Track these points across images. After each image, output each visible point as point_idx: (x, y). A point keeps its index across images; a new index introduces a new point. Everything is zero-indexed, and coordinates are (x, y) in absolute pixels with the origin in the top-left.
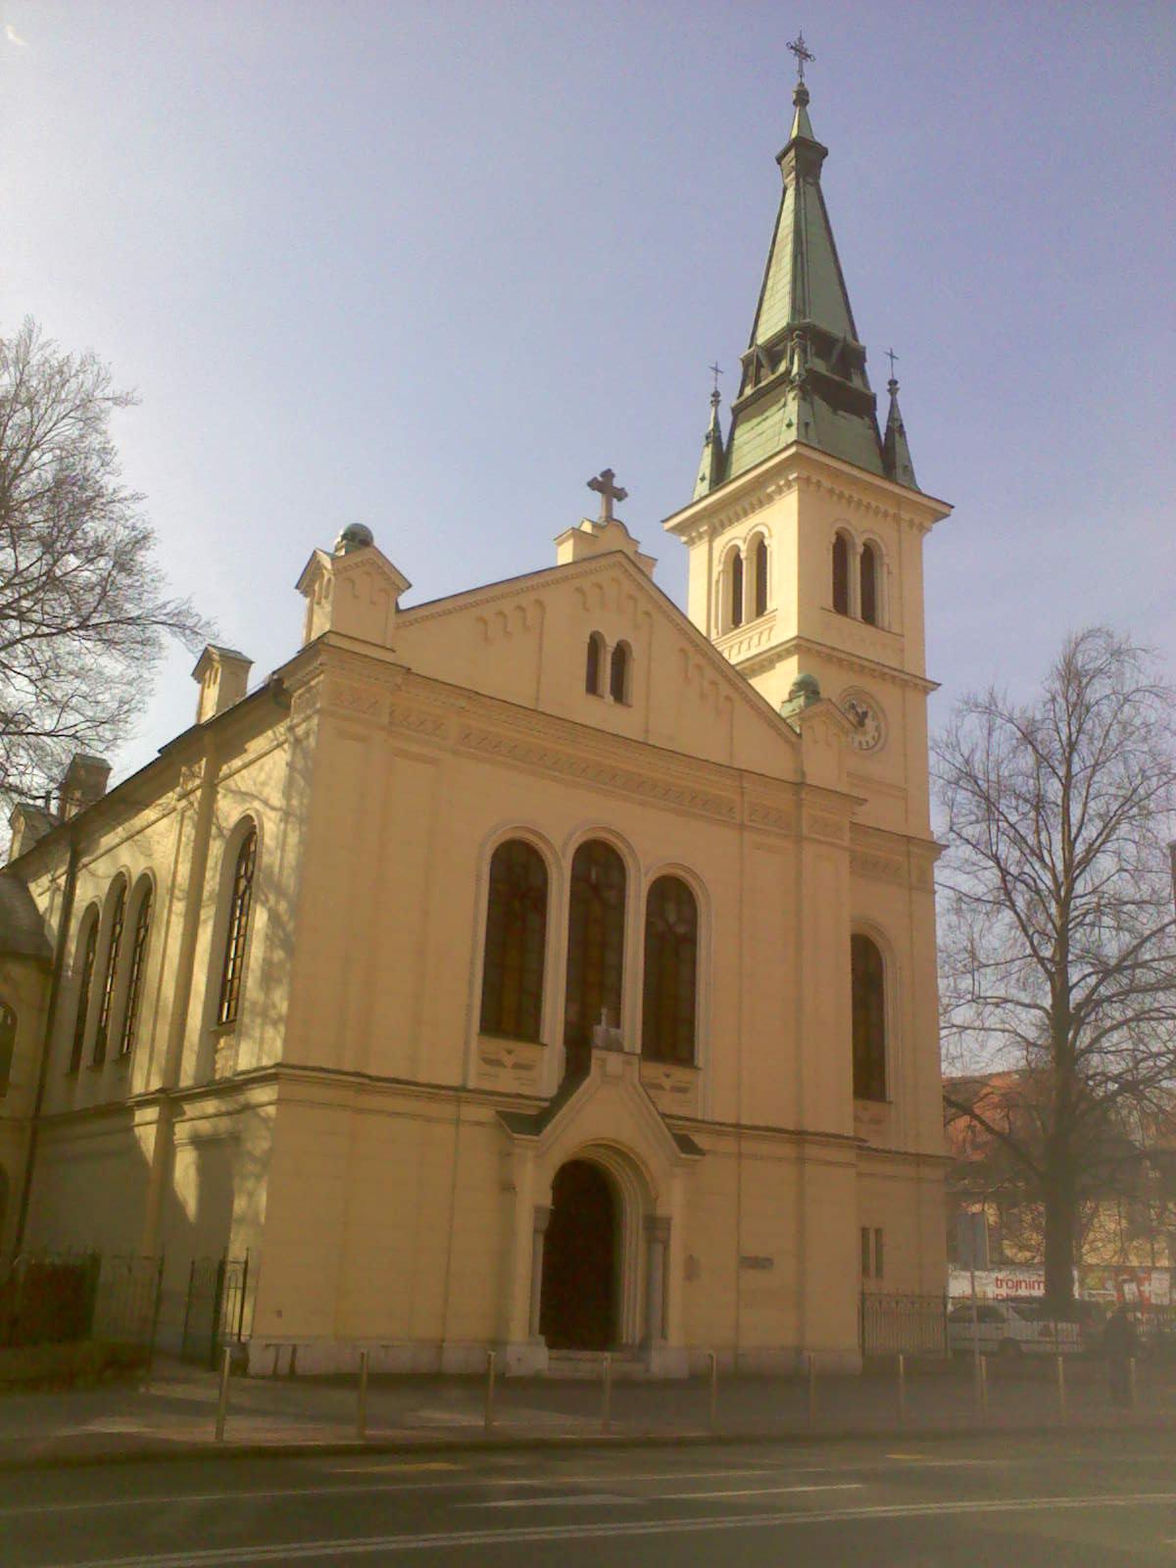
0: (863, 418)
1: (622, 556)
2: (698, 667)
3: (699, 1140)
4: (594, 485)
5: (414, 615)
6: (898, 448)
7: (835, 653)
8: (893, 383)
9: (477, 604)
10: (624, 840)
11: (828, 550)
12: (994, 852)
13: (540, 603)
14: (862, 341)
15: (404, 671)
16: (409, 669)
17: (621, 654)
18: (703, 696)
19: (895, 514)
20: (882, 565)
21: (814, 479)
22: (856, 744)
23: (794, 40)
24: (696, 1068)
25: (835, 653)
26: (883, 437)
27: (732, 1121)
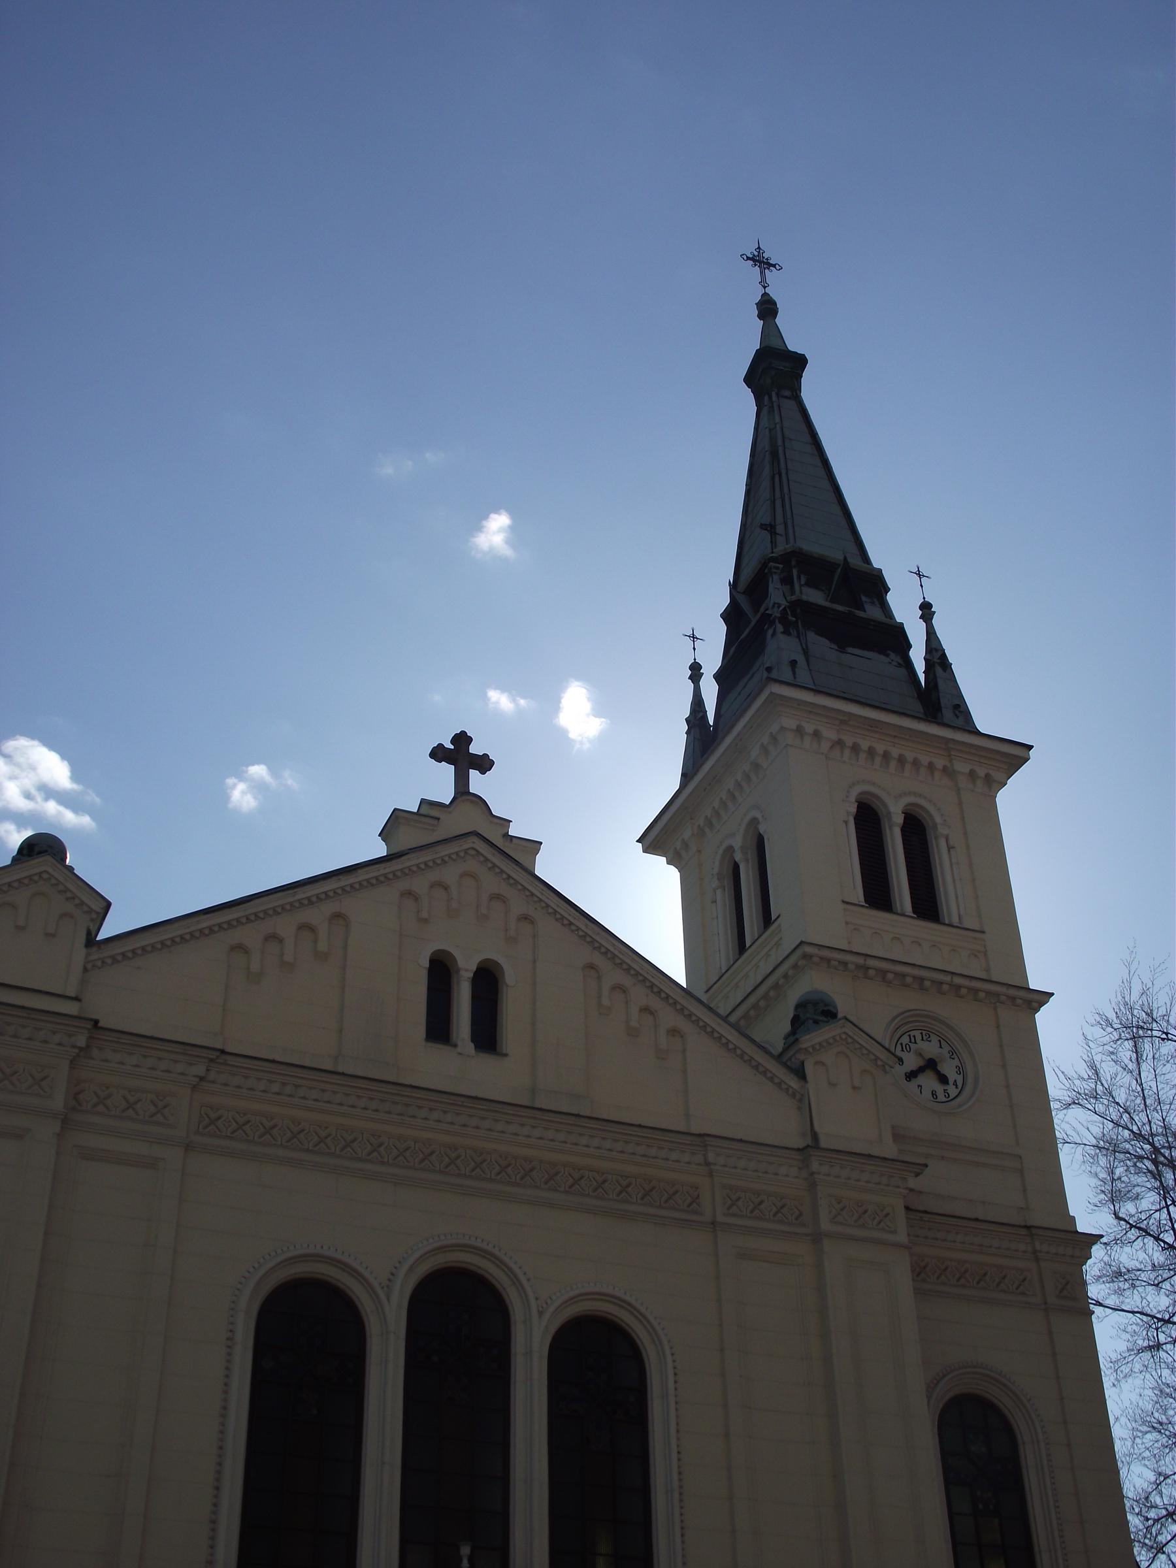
0: (887, 655)
1: (475, 839)
2: (618, 988)
4: (438, 754)
5: (118, 948)
7: (871, 962)
8: (926, 611)
9: (230, 925)
11: (846, 822)
13: (338, 916)
14: (876, 564)
15: (89, 1025)
17: (488, 980)
20: (936, 838)
22: (927, 1094)
23: (750, 250)
25: (871, 962)
26: (922, 678)
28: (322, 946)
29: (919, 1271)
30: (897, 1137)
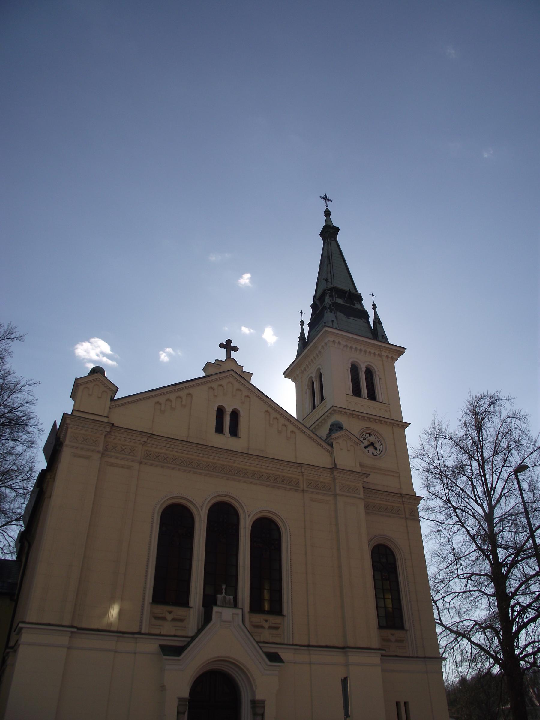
3: (283, 655)
4: (222, 346)
5: (121, 402)
6: (378, 329)
7: (354, 412)
10: (237, 501)
12: (483, 515)
15: (111, 425)
16: (113, 424)
17: (235, 415)
18: (280, 432)
19: (379, 354)
21: (337, 341)
23: (323, 195)
24: (284, 616)
25: (354, 412)
27: (306, 643)
28: (184, 403)
29: (367, 506)
30: (361, 465)
